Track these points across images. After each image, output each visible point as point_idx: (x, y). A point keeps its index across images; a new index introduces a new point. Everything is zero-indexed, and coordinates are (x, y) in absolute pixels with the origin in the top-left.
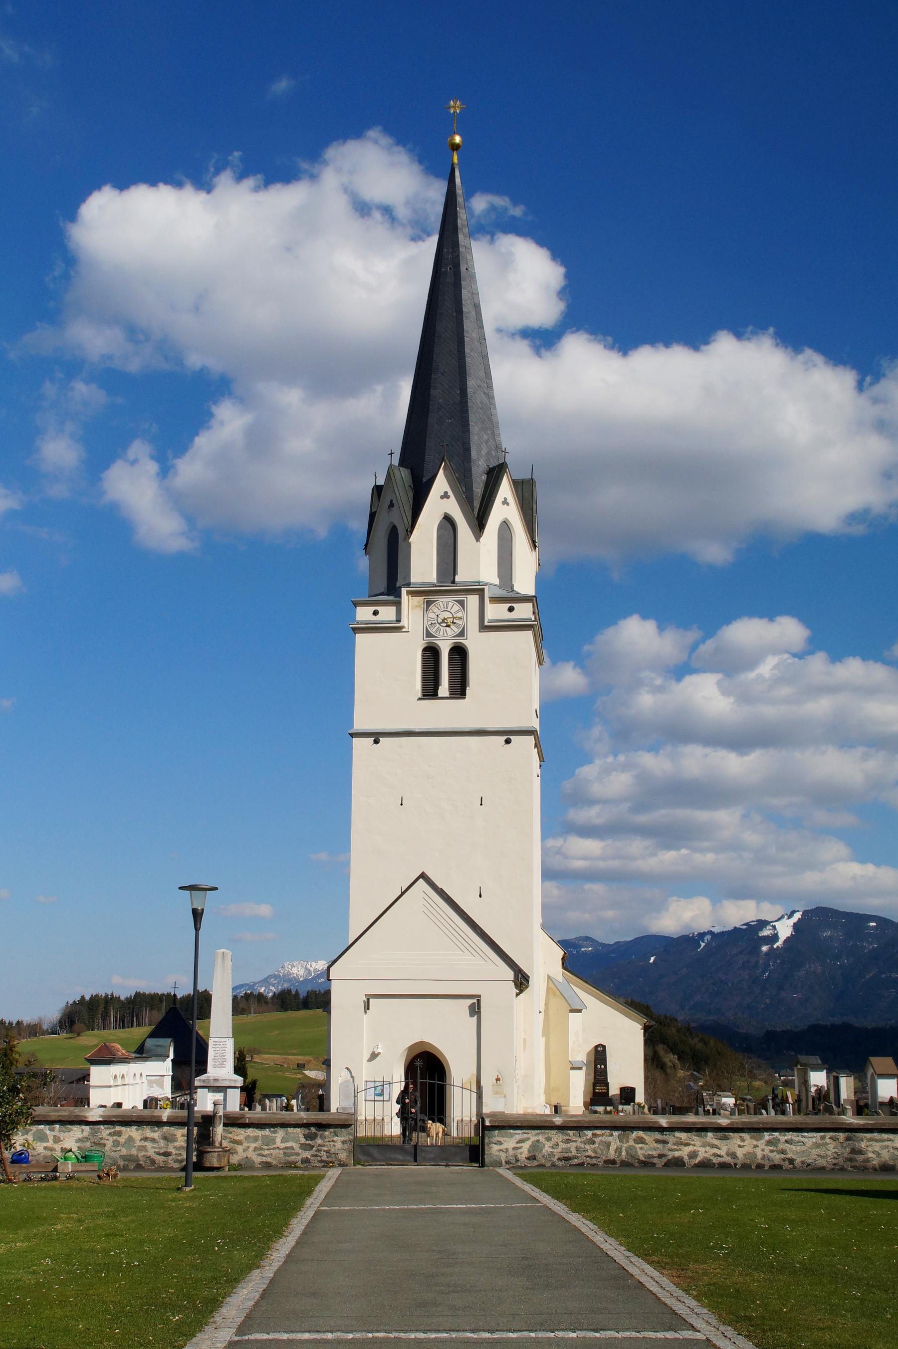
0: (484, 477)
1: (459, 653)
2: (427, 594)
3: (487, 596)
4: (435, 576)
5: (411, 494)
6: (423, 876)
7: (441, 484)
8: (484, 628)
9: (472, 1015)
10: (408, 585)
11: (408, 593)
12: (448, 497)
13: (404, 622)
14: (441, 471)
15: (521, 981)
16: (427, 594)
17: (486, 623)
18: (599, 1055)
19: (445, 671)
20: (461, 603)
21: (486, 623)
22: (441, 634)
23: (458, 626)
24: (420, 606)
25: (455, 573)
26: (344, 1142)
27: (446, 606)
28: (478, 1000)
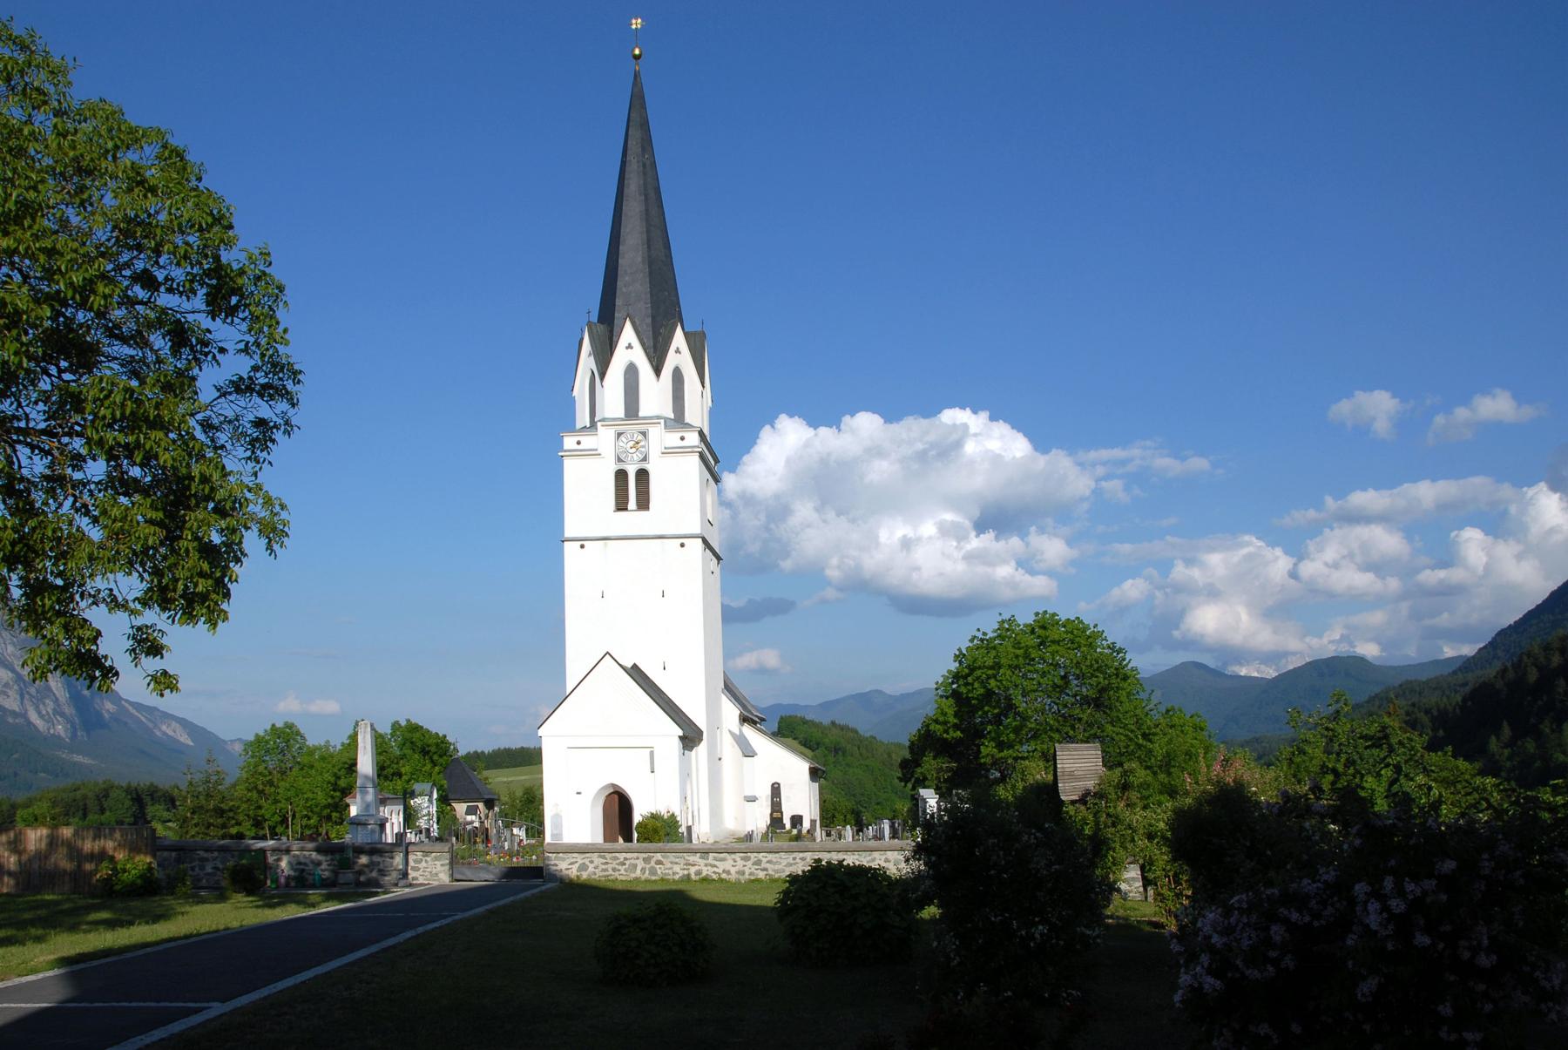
1: (643, 475)
7: (628, 334)
15: (691, 737)
18: (776, 790)
19: (632, 489)
26: (1436, 806)
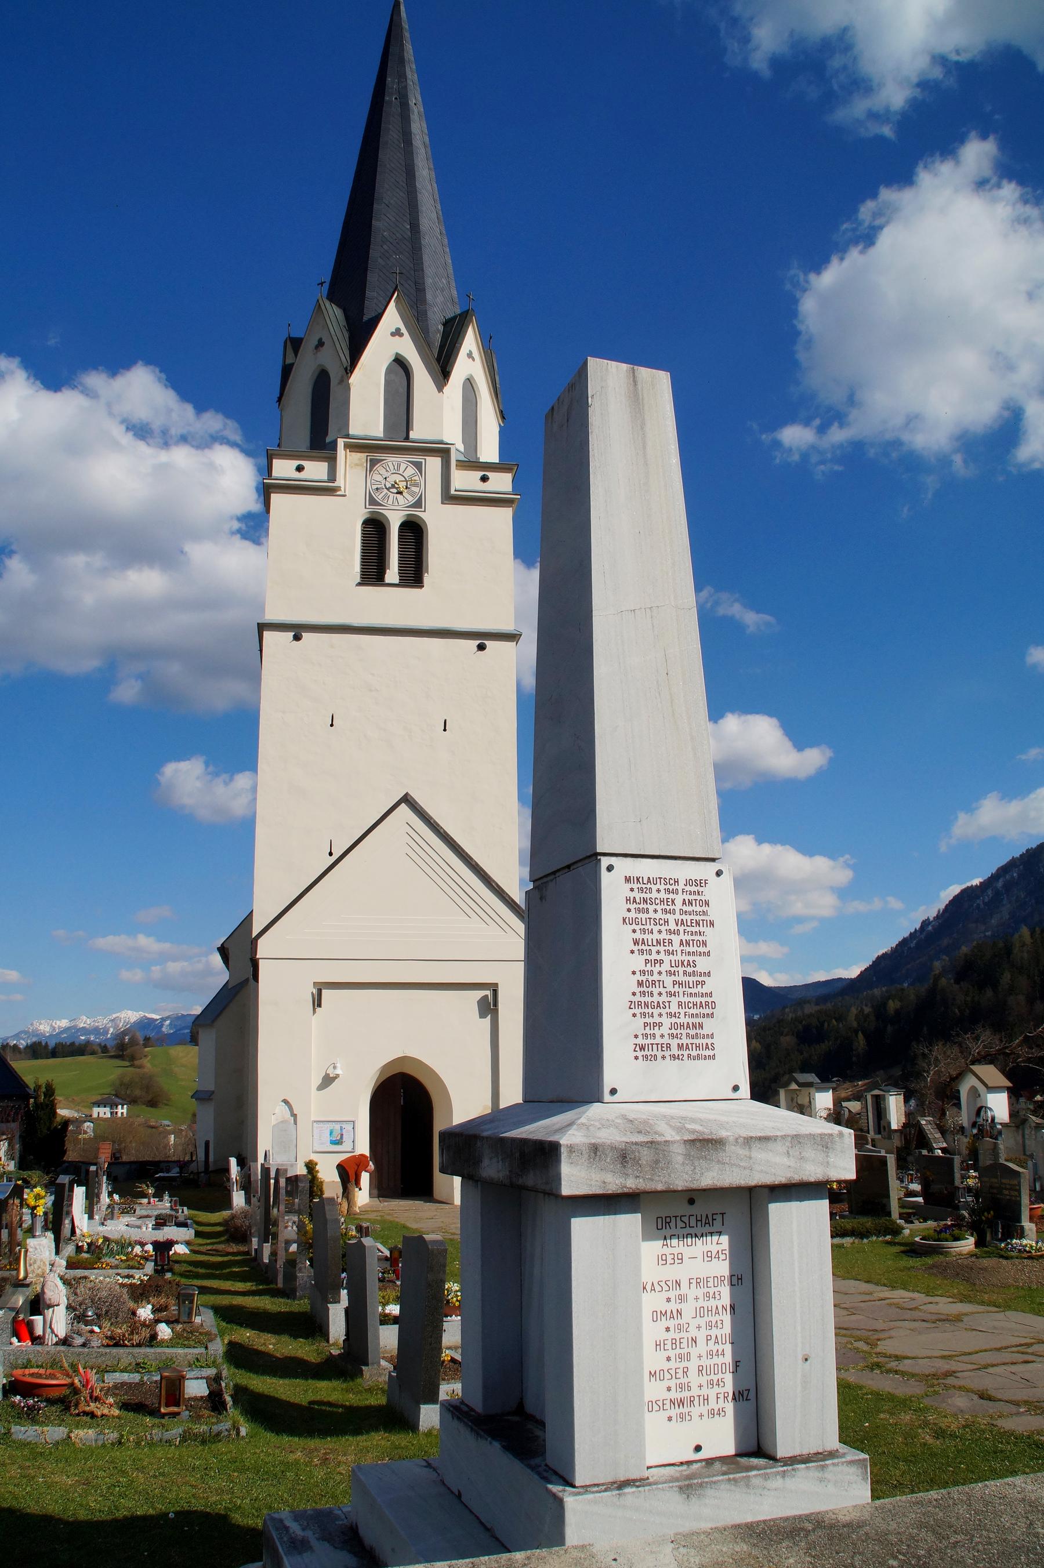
0: (441, 328)
1: (414, 532)
2: (371, 450)
3: (454, 457)
4: (381, 428)
5: (347, 335)
6: (406, 799)
7: (391, 318)
8: (449, 498)
9: (482, 1015)
10: (347, 436)
11: (347, 446)
12: (401, 335)
13: (340, 482)
14: (392, 304)
16: (371, 450)
17: (453, 492)
19: (395, 551)
20: (418, 466)
21: (453, 492)
22: (390, 502)
23: (413, 494)
24: (361, 465)
25: (408, 427)
27: (397, 468)
28: (495, 992)
